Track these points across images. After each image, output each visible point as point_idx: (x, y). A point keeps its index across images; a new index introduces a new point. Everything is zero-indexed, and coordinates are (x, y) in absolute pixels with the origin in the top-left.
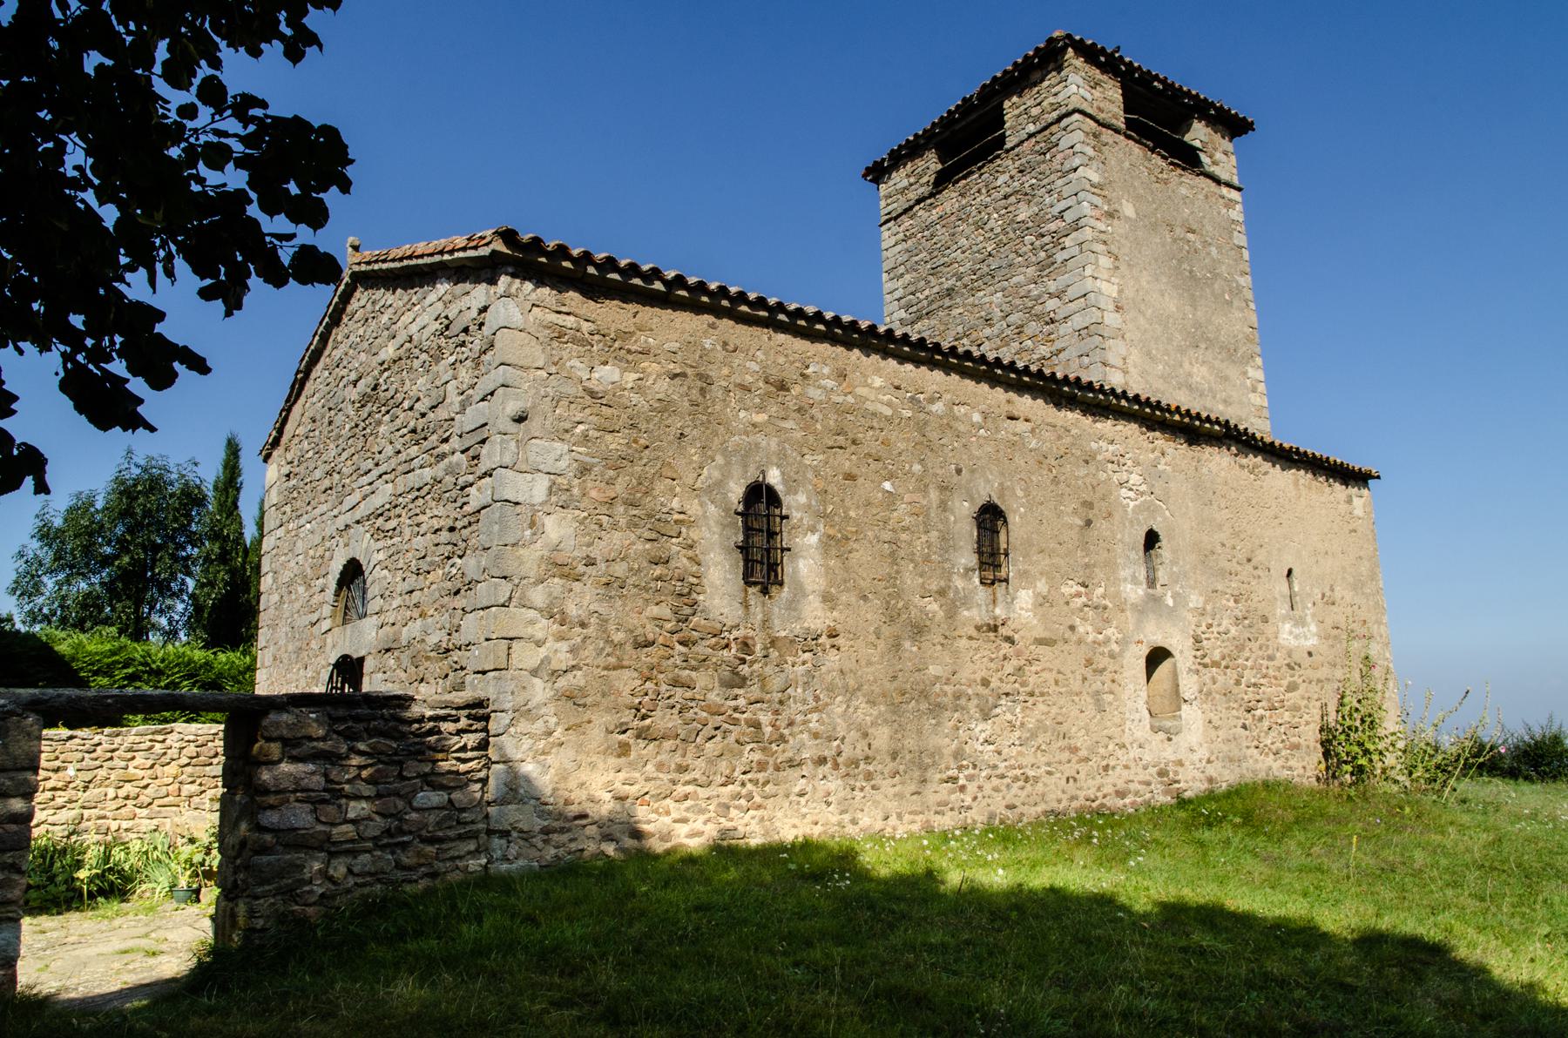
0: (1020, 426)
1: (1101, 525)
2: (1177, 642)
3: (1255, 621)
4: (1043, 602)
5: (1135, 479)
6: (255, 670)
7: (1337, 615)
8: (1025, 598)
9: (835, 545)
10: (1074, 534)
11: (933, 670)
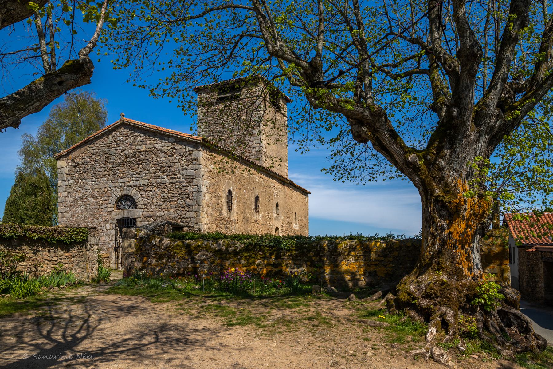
0: (262, 180)
1: (271, 201)
2: (280, 227)
3: (290, 223)
4: (263, 216)
5: (276, 192)
6: (362, 237)
7: (302, 223)
8: (261, 215)
9: (238, 202)
10: (267, 203)
11: (249, 228)
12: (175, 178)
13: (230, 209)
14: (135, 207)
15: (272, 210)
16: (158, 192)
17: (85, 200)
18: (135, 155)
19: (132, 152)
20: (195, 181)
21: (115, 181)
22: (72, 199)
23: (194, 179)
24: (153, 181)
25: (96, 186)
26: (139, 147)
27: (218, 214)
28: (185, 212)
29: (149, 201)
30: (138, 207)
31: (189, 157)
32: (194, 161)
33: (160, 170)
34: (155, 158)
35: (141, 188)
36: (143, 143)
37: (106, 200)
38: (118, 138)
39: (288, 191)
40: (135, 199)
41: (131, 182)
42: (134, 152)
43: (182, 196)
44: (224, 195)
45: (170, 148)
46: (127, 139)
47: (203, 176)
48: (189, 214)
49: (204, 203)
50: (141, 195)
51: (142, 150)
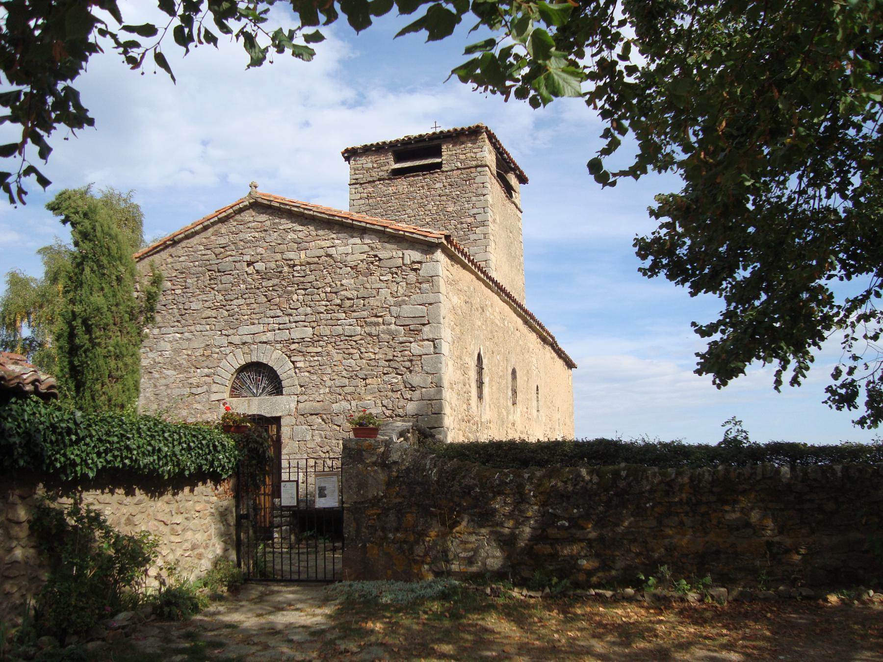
12: (377, 324)
13: (480, 397)
20: (426, 329)
21: (231, 332)
23: (424, 325)
26: (291, 255)
27: (465, 406)
31: (412, 276)
35: (293, 347)
44: (472, 363)
51: (297, 262)
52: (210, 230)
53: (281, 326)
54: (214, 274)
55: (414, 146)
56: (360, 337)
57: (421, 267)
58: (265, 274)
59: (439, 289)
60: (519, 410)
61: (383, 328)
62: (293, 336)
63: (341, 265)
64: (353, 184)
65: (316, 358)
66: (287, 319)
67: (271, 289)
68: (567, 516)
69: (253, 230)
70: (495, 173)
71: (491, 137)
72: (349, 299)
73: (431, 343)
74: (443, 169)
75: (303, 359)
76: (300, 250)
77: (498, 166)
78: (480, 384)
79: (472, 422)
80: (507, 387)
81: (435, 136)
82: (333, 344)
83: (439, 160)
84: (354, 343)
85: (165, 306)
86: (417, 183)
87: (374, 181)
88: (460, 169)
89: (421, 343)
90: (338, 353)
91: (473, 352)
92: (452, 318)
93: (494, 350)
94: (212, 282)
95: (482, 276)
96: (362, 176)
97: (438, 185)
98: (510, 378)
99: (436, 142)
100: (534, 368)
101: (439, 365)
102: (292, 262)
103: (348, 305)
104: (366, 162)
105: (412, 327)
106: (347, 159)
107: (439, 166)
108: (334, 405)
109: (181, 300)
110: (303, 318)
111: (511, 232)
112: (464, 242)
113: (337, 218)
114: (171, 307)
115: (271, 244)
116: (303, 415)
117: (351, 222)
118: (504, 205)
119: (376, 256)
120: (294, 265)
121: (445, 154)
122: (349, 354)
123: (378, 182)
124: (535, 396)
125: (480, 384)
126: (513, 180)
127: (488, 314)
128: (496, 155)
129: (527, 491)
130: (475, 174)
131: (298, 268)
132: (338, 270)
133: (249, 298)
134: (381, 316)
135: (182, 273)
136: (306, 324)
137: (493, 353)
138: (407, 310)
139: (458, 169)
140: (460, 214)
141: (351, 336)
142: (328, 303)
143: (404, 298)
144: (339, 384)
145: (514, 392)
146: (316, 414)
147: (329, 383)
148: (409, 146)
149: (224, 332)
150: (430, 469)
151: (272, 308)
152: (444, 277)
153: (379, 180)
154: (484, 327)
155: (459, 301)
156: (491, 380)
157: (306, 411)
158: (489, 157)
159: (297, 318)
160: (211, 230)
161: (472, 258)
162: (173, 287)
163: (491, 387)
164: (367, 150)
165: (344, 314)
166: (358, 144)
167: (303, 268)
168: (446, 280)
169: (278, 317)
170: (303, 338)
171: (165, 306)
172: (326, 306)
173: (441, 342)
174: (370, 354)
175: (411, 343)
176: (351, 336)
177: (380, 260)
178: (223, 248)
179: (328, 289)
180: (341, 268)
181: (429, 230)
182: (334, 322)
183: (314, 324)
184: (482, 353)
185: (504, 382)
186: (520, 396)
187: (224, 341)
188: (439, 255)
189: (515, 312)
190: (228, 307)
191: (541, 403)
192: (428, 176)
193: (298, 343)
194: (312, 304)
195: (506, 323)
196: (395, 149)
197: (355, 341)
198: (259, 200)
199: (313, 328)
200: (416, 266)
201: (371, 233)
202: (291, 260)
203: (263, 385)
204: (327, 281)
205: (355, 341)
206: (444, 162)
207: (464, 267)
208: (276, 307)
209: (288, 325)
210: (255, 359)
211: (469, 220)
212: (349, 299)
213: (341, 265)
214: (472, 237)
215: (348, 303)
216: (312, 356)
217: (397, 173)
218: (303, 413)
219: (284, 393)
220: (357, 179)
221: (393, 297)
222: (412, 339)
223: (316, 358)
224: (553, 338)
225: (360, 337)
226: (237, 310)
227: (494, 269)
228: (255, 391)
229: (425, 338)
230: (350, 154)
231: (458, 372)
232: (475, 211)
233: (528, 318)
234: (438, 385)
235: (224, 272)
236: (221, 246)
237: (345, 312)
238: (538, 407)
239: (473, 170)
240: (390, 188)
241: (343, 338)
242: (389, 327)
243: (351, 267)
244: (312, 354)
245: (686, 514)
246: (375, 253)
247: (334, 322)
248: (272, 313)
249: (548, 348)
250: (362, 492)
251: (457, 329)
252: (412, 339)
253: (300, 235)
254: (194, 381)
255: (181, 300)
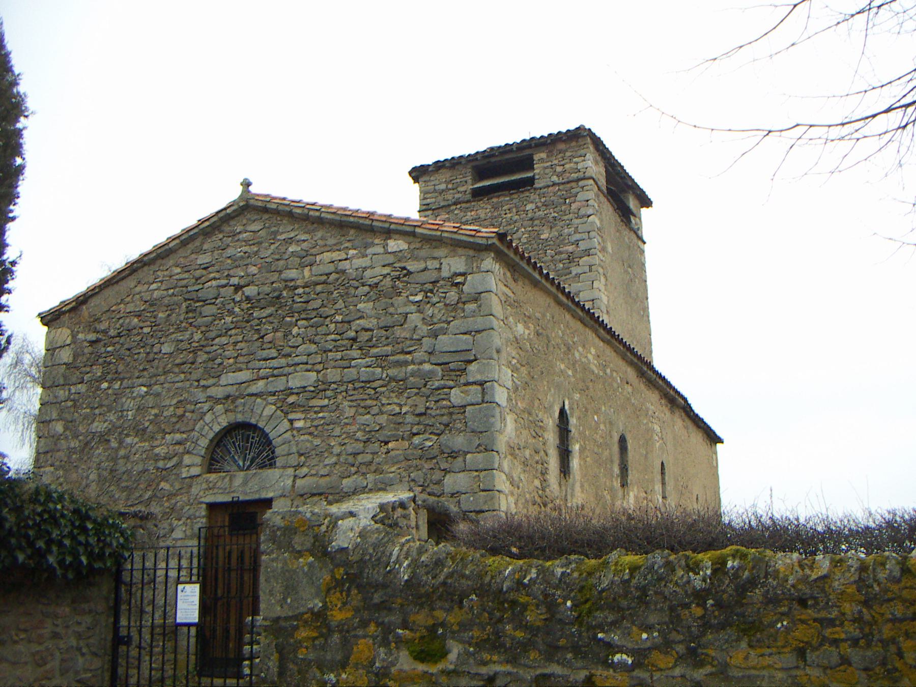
12: (406, 363)
13: (565, 469)
14: (270, 462)
15: (653, 481)
16: (350, 412)
17: (114, 444)
18: (278, 298)
19: (267, 289)
20: (473, 367)
21: (211, 381)
22: (74, 444)
23: (470, 362)
24: (333, 374)
25: (151, 401)
26: (292, 274)
27: (537, 483)
28: (437, 475)
29: (317, 442)
30: (279, 462)
31: (453, 295)
32: (471, 306)
33: (354, 340)
34: (340, 304)
35: (292, 399)
36: (305, 259)
37: (179, 443)
38: (230, 252)
39: (679, 423)
40: (271, 436)
41: (261, 383)
42: (274, 290)
43: (430, 421)
44: (551, 422)
45: (386, 270)
46: (256, 253)
47: (498, 351)
48: (451, 482)
49: (501, 443)
50: (291, 421)
51: (299, 283)
52: (190, 246)
53: (276, 372)
54: (193, 304)
55: (499, 159)
56: (380, 382)
57: (466, 279)
58: (259, 301)
59: (491, 309)
60: (631, 494)
61: (412, 369)
62: (290, 384)
63: (356, 284)
64: (423, 211)
65: (321, 415)
66: (283, 361)
67: (264, 320)
68: (630, 645)
69: (244, 243)
70: (604, 189)
71: (598, 143)
72: (367, 330)
73: (479, 388)
74: (536, 186)
75: (303, 416)
76: (302, 266)
77: (607, 181)
78: (565, 454)
79: (550, 505)
80: (612, 461)
81: (525, 144)
82: (344, 394)
83: (530, 174)
84: (373, 392)
85: (129, 350)
86: (502, 206)
87: (449, 206)
88: (558, 184)
89: (466, 388)
90: (350, 407)
91: (551, 406)
92: (514, 354)
93: (589, 407)
94: (190, 315)
95: (564, 299)
96: (433, 200)
97: (530, 207)
98: (616, 448)
99: (527, 152)
100: (657, 438)
101: (492, 420)
102: (292, 284)
103: (366, 338)
104: (440, 181)
105: (452, 366)
106: (416, 180)
107: (530, 182)
108: (345, 481)
109: (151, 341)
110: (304, 359)
111: (630, 267)
112: (564, 278)
113: (352, 219)
114: (137, 351)
115: (267, 260)
116: (302, 496)
117: (370, 222)
118: (618, 231)
119: (404, 268)
120: (296, 288)
121: (538, 168)
122: (365, 407)
123: (454, 207)
124: (659, 477)
125: (565, 454)
126: (632, 203)
127: (577, 355)
128: (606, 167)
129: (560, 600)
130: (578, 189)
131: (300, 291)
132: (352, 291)
133: (236, 335)
134: (409, 353)
135: (151, 305)
136: (309, 367)
137: (587, 410)
138: (445, 342)
139: (554, 184)
140: (560, 240)
141: (369, 382)
142: (338, 337)
143: (442, 325)
144: (350, 451)
145: (624, 469)
146: (320, 494)
147: (337, 450)
148: (493, 160)
149: (202, 383)
150: (397, 561)
151: (264, 346)
152: (500, 295)
153: (455, 204)
154: (570, 373)
155: (527, 332)
156: (582, 450)
157: (305, 490)
158: (592, 166)
159: (297, 360)
160: (191, 246)
161: (545, 272)
162: (142, 324)
163: (582, 458)
164: (439, 166)
165: (359, 352)
166: (429, 159)
167: (307, 290)
168: (503, 299)
169: (273, 358)
170: (305, 387)
171: (129, 350)
172: (335, 341)
173: (492, 386)
174: (394, 406)
175: (451, 388)
176: (369, 382)
177: (409, 273)
178: (205, 269)
179: (339, 318)
180: (357, 288)
181: (476, 228)
182: (345, 363)
183: (320, 367)
184: (567, 407)
185: (607, 453)
186: (632, 476)
187: (201, 396)
188: (489, 262)
189: (624, 358)
190: (208, 349)
191: (669, 488)
192: (515, 196)
193: (297, 394)
194: (317, 339)
195: (608, 371)
196: (474, 164)
197: (375, 389)
198: (252, 202)
199: (318, 372)
200: (459, 279)
201: (397, 236)
202: (293, 280)
203: (252, 454)
204: (337, 306)
205: (375, 389)
206: (537, 177)
207: (535, 284)
208: (270, 346)
209: (287, 370)
210: (240, 418)
211: (570, 248)
212: (367, 330)
213: (356, 284)
214: (575, 270)
215: (364, 336)
216: (316, 412)
217: (478, 194)
218: (302, 492)
219: (278, 464)
220: (428, 204)
221: (426, 324)
222: (451, 383)
223: (321, 415)
224: (685, 400)
225: (380, 382)
226: (220, 351)
227: (605, 311)
228: (241, 463)
229: (471, 380)
230: (418, 173)
231: (525, 432)
232: (578, 236)
233: (645, 368)
234: (488, 447)
235: (204, 301)
236: (202, 266)
237: (360, 349)
238: (664, 492)
239: (574, 184)
240: (469, 214)
241: (357, 385)
242: (421, 367)
243: (370, 286)
244: (316, 409)
245: (855, 642)
246: (403, 265)
247: (345, 363)
248: (265, 354)
249: (678, 414)
250: (289, 601)
251: (524, 371)
252: (451, 383)
253: (305, 245)
254: (161, 451)
255: (151, 341)
